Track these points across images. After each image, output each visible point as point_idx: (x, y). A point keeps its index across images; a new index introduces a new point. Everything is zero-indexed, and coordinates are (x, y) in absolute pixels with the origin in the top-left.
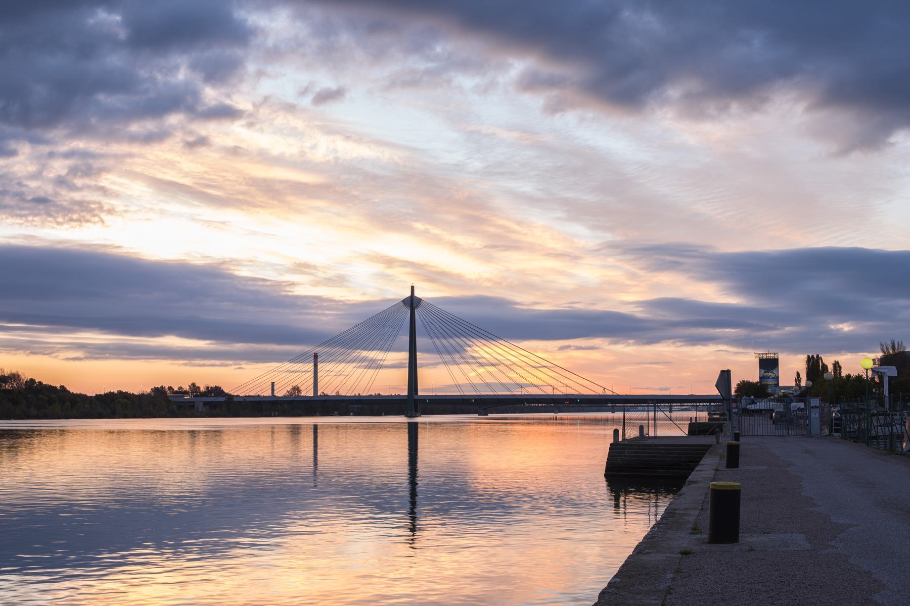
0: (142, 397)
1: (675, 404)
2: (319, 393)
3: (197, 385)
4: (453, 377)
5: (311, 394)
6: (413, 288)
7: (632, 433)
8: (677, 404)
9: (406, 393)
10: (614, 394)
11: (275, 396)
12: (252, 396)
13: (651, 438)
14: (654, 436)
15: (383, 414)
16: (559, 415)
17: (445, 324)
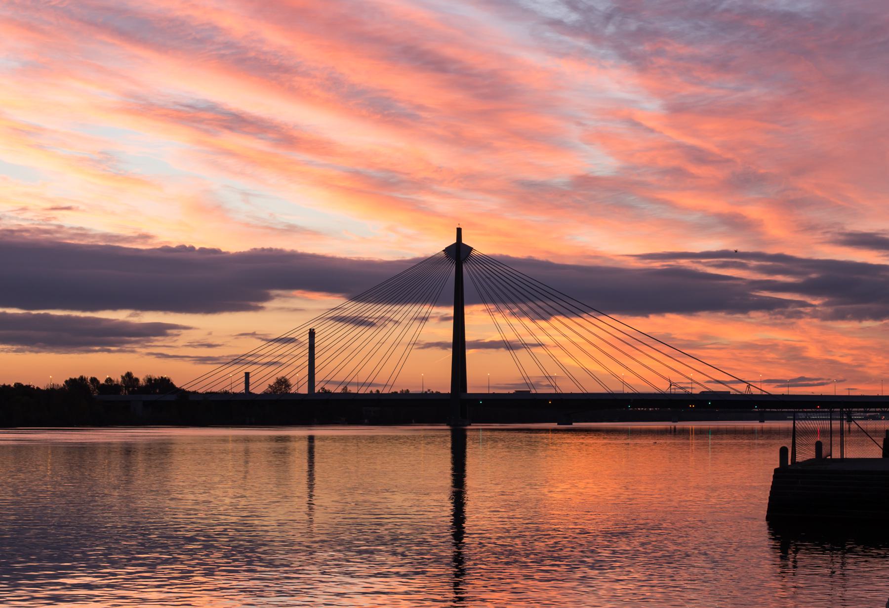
0: (52, 392)
1: (856, 410)
2: (317, 389)
3: (135, 375)
4: (598, 381)
5: (304, 390)
6: (459, 231)
7: (806, 454)
8: (860, 409)
9: (448, 390)
10: (764, 393)
11: (251, 393)
12: (214, 393)
13: (836, 460)
14: (840, 457)
15: (413, 421)
16: (680, 425)
17: (500, 280)
